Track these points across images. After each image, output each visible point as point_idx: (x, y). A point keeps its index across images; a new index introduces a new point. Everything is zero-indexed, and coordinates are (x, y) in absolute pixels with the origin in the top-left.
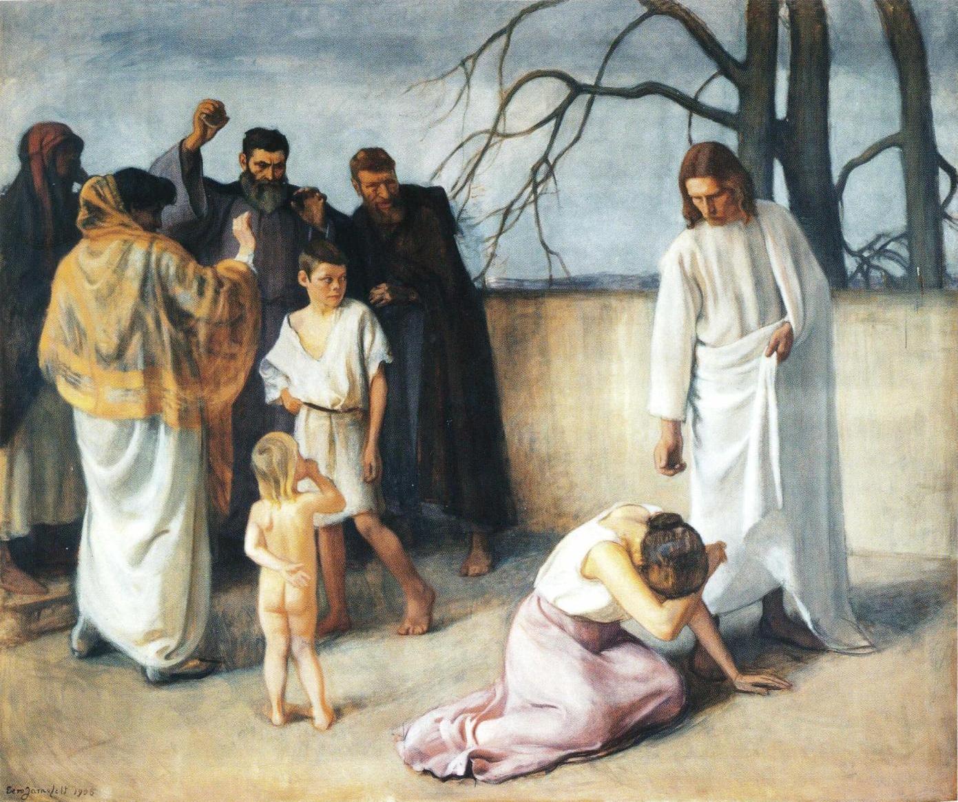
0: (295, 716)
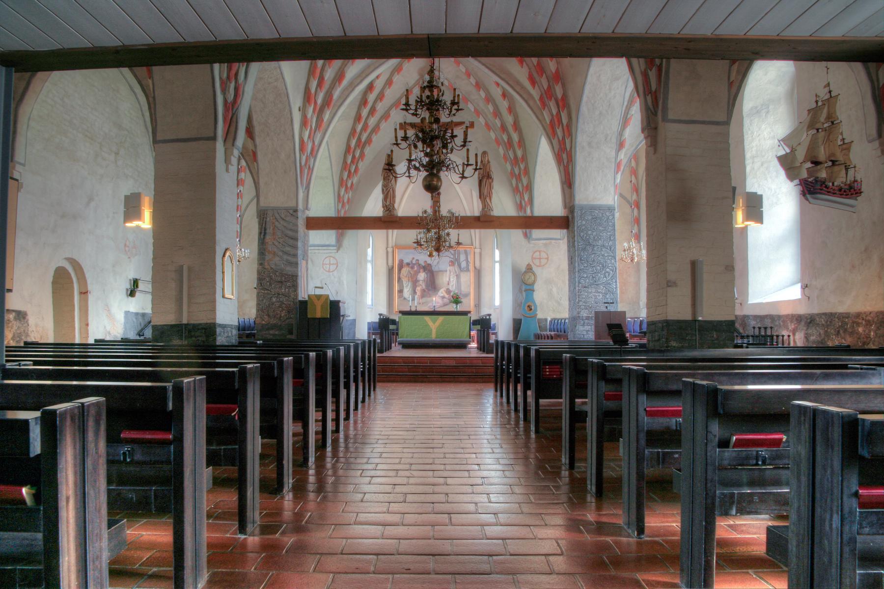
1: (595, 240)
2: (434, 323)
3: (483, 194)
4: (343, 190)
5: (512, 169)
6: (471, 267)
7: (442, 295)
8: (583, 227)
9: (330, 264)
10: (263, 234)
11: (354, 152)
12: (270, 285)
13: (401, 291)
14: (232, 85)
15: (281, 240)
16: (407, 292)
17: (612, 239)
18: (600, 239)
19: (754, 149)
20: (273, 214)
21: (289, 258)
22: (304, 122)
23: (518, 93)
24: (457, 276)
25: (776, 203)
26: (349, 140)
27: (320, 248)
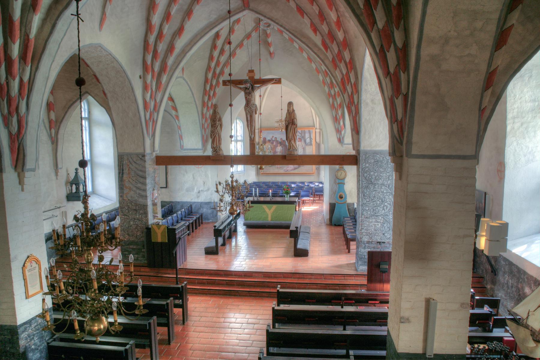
0: (278, 168)
1: (376, 179)
2: (270, 210)
4: (205, 109)
5: (329, 91)
8: (367, 169)
10: (121, 174)
11: (211, 81)
12: (129, 212)
14: (15, 120)
15: (134, 179)
17: (390, 178)
18: (381, 179)
19: (516, 110)
20: (128, 158)
21: (141, 192)
22: (145, 87)
24: (303, 148)
25: (532, 160)
26: (206, 74)
27: (191, 151)
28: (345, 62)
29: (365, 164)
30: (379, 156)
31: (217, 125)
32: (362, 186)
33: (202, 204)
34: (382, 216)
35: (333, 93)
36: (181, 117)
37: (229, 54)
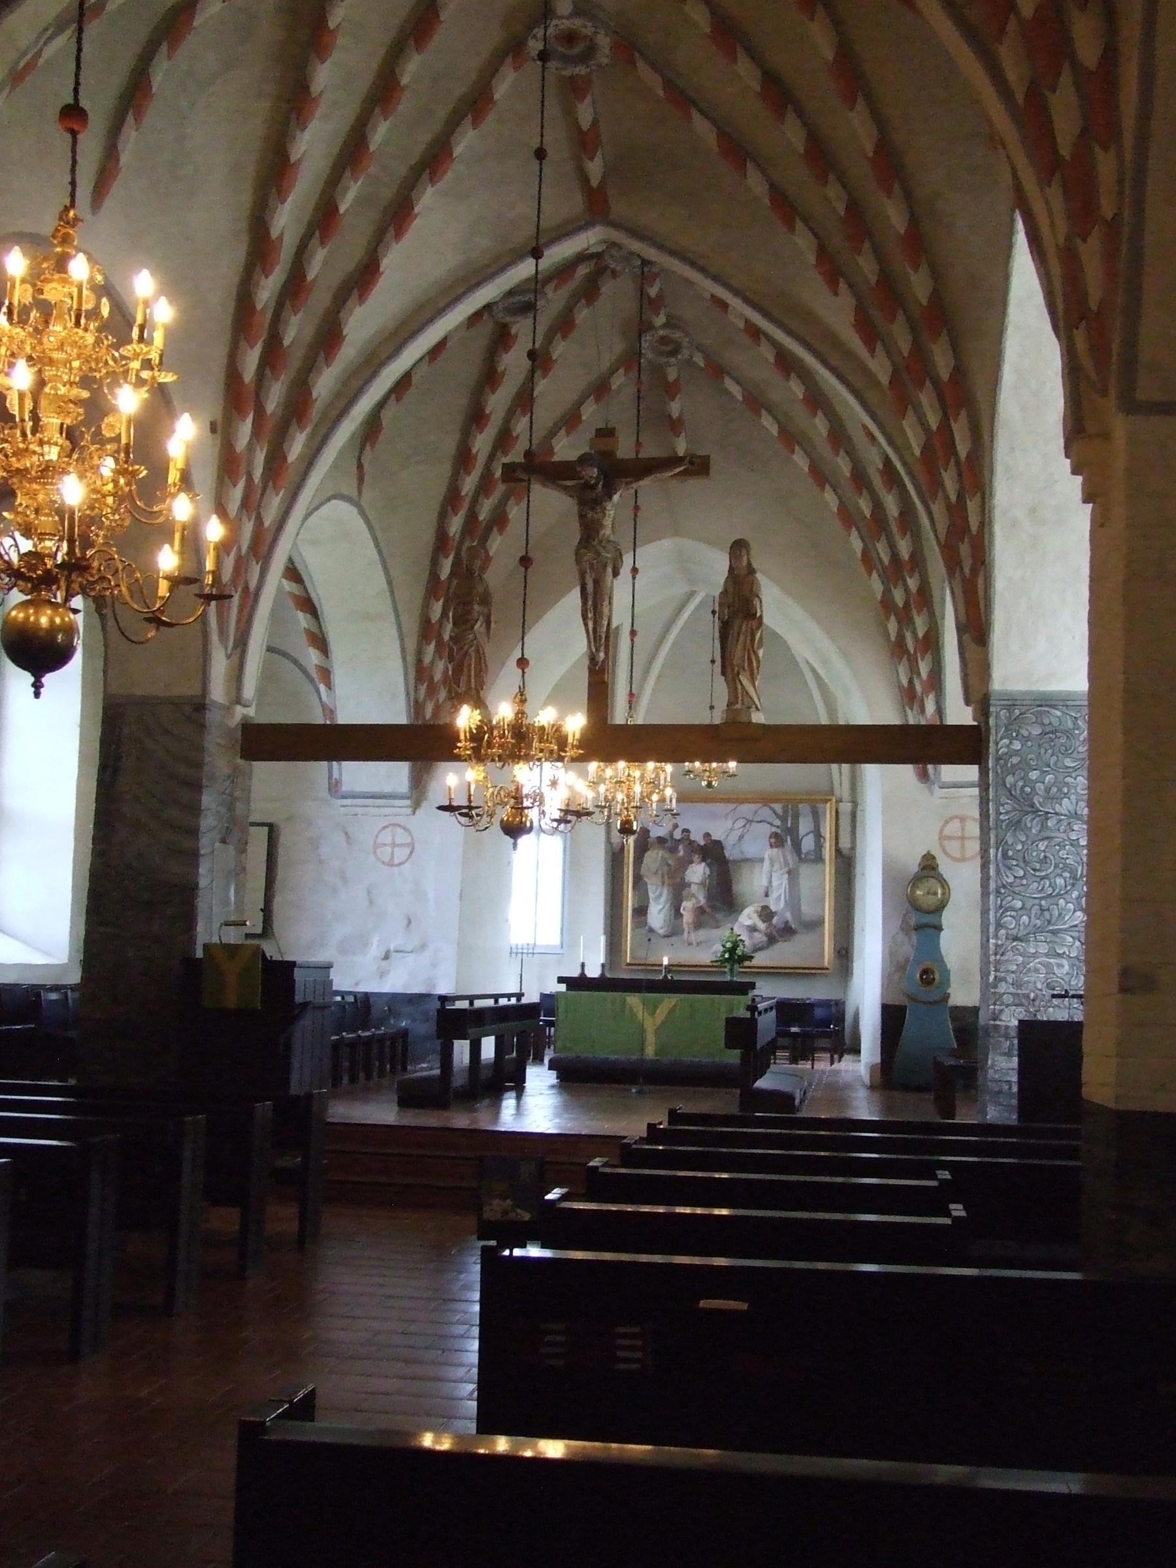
0: (690, 944)
1: (1049, 798)
3: (732, 664)
4: (431, 649)
5: (887, 593)
6: (828, 852)
7: (749, 923)
8: (1015, 760)
9: (394, 845)
13: (641, 911)
16: (657, 916)
23: (833, 370)
24: (789, 872)
26: (443, 517)
28: (936, 383)
29: (1006, 741)
30: (1059, 713)
31: (475, 615)
32: (997, 820)
33: (396, 1000)
34: (1074, 934)
35: (899, 597)
36: (338, 677)
37: (526, 638)
